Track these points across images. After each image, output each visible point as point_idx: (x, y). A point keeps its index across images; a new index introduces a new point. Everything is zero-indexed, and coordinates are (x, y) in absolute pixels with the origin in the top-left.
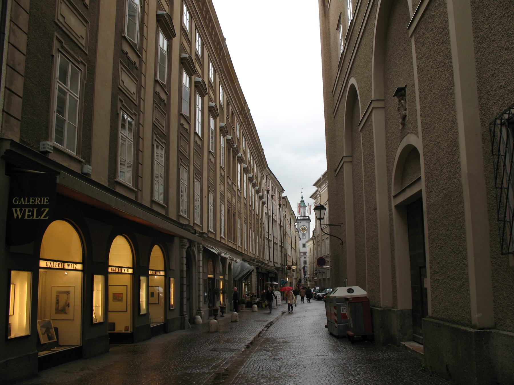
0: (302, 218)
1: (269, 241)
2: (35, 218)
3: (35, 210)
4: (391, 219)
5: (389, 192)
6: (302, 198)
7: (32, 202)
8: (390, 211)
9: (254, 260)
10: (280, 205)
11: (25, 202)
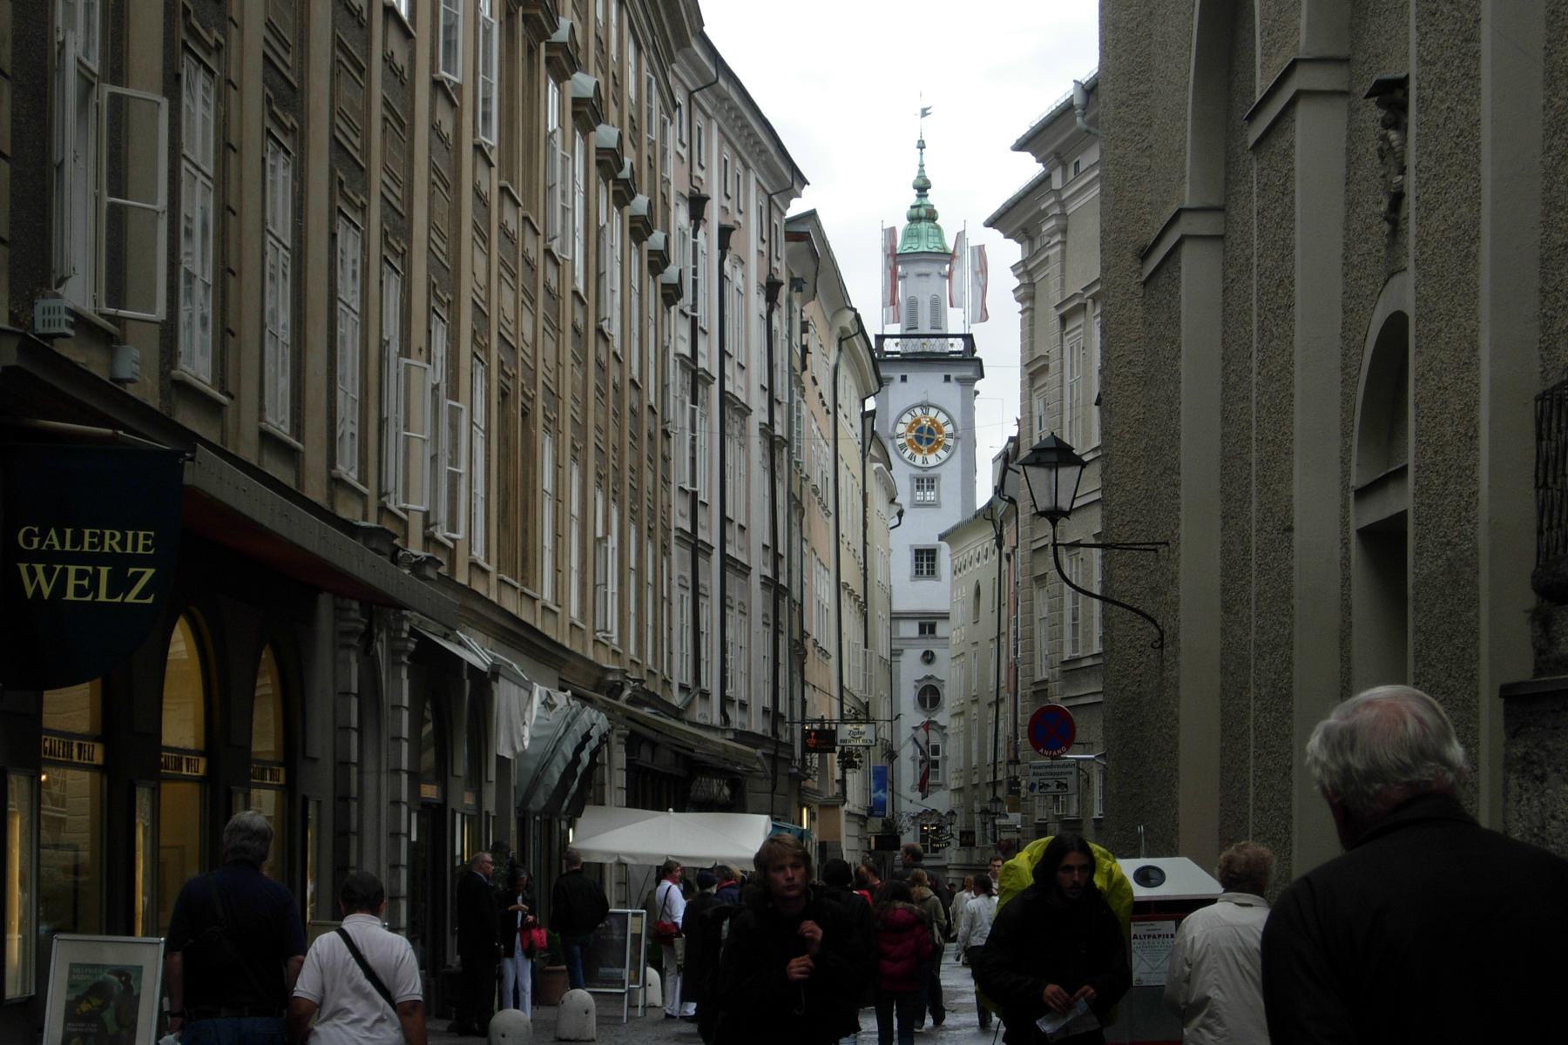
0: (914, 346)
1: (698, 549)
2: (102, 597)
3: (104, 571)
4: (1346, 580)
5: (1346, 473)
6: (922, 188)
7: (92, 545)
8: (1345, 544)
9: (615, 690)
10: (771, 289)
11: (62, 544)
